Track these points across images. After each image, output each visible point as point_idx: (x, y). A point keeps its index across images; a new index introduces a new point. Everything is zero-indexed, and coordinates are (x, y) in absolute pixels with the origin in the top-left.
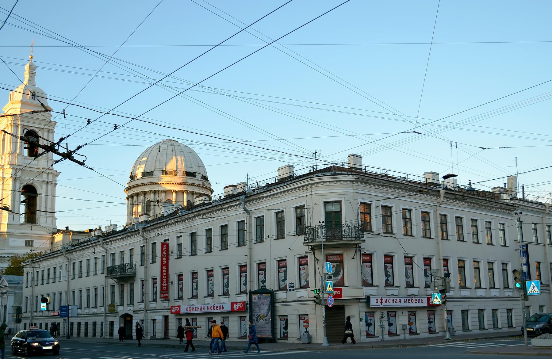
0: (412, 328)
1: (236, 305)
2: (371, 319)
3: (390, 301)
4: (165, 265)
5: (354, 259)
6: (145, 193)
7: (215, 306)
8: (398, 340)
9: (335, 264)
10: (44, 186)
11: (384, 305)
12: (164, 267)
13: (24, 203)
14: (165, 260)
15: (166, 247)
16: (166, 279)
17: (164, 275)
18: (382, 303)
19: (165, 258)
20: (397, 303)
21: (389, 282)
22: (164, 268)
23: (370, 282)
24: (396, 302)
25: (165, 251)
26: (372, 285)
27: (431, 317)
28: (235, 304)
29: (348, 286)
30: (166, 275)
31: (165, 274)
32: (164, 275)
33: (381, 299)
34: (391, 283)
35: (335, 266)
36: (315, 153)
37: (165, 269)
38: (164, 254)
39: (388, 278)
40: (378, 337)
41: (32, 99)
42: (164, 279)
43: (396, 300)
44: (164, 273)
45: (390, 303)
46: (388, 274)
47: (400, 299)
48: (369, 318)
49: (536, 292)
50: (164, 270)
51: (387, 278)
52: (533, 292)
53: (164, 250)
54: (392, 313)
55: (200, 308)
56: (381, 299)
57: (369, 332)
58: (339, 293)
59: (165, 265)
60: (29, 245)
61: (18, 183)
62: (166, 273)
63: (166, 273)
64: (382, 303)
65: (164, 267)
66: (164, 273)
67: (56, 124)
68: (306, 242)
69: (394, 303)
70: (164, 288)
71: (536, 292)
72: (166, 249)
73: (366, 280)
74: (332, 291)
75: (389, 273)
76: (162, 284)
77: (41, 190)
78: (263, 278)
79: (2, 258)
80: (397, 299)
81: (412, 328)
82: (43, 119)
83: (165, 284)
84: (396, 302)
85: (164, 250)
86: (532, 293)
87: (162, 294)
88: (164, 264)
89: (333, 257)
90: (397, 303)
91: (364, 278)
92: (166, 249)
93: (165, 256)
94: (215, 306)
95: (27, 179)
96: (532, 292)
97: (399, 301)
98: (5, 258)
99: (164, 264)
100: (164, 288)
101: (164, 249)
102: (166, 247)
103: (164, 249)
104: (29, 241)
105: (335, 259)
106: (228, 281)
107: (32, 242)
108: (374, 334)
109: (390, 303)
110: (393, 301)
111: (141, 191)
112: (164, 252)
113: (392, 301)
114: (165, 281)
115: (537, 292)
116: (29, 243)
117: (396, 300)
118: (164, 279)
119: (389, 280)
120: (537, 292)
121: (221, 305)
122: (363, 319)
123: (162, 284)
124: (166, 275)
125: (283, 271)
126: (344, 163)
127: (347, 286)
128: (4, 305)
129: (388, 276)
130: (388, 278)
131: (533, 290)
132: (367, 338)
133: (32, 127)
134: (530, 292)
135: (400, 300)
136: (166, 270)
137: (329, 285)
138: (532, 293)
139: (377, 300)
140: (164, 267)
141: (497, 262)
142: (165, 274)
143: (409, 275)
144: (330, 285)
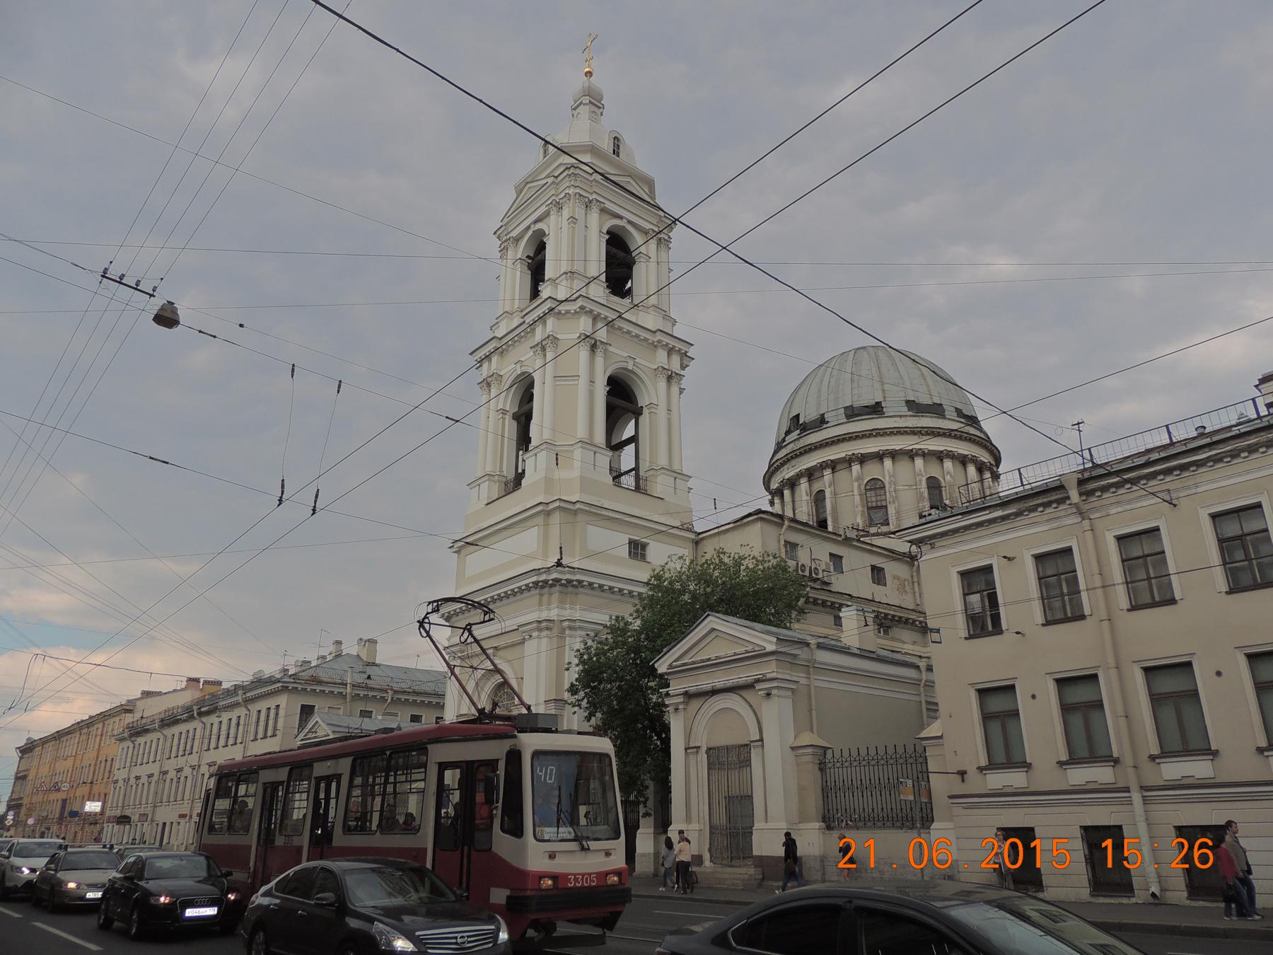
6: (863, 459)
10: (662, 384)
41: (614, 153)
61: (599, 360)
77: (650, 393)
79: (570, 589)
95: (622, 355)
98: (581, 590)
107: (644, 546)
111: (853, 454)
116: (637, 550)
128: (704, 749)
133: (621, 217)
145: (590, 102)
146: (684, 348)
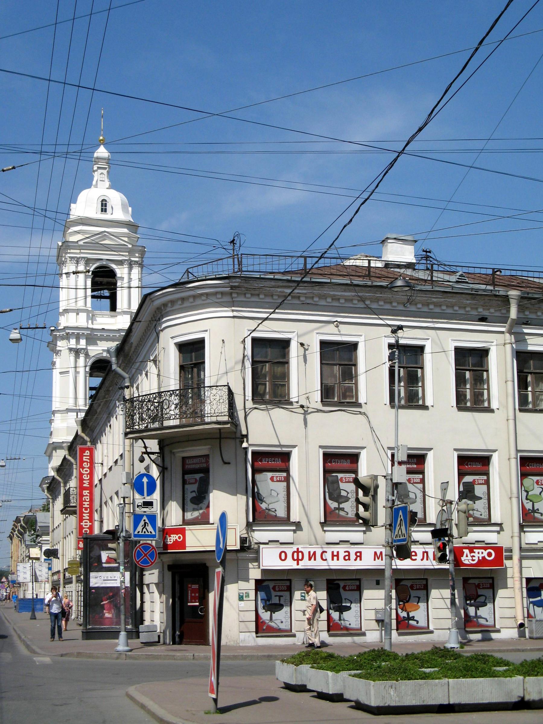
0: (413, 617)
2: (280, 597)
3: (328, 556)
5: (229, 463)
8: (233, 647)
9: (198, 476)
11: (306, 564)
12: (86, 492)
14: (86, 478)
15: (88, 454)
16: (88, 515)
17: (84, 506)
18: (298, 560)
19: (87, 474)
20: (349, 559)
21: (342, 513)
22: (85, 494)
23: (281, 513)
24: (347, 558)
26: (286, 521)
27: (479, 593)
29: (213, 524)
30: (88, 506)
31: (87, 505)
32: (84, 506)
33: (298, 551)
34: (350, 515)
35: (198, 480)
36: (233, 242)
37: (87, 496)
38: (86, 466)
39: (339, 503)
40: (294, 636)
41: (102, 211)
42: (84, 515)
43: (347, 554)
44: (84, 503)
45: (326, 560)
46: (339, 496)
47: (360, 553)
48: (273, 593)
49: (148, 532)
50: (84, 497)
51: (337, 504)
52: (145, 532)
53: (84, 460)
54: (484, 581)
56: (298, 551)
57: (272, 624)
58: (179, 538)
59: (86, 489)
62: (88, 503)
63: (88, 503)
64: (298, 560)
66: (84, 503)
69: (338, 559)
71: (148, 532)
72: (88, 457)
73: (269, 510)
74: (153, 533)
75: (343, 493)
76: (81, 524)
80: (349, 552)
81: (413, 617)
82: (117, 243)
83: (87, 522)
84: (347, 558)
85: (84, 460)
86: (143, 533)
88: (84, 485)
89: (195, 461)
90: (349, 559)
91: (264, 506)
92: (88, 457)
93: (86, 471)
96: (143, 532)
97: (357, 556)
99: (84, 485)
101: (84, 457)
102: (88, 454)
103: (84, 457)
105: (197, 466)
108: (288, 627)
109: (326, 560)
110: (338, 556)
112: (86, 463)
113: (333, 556)
114: (88, 518)
115: (150, 533)
117: (347, 554)
118: (84, 515)
119: (344, 508)
120: (150, 533)
122: (248, 595)
123: (91, 524)
124: (88, 506)
126: (242, 254)
127: (212, 523)
129: (340, 501)
130: (339, 503)
131: (145, 529)
132: (257, 637)
134: (139, 532)
135: (358, 554)
136: (88, 497)
137: (142, 523)
138: (143, 533)
139: (425, 554)
140: (86, 492)
141: (499, 456)
142: (87, 505)
143: (412, 496)
144: (147, 521)
145: (98, 167)
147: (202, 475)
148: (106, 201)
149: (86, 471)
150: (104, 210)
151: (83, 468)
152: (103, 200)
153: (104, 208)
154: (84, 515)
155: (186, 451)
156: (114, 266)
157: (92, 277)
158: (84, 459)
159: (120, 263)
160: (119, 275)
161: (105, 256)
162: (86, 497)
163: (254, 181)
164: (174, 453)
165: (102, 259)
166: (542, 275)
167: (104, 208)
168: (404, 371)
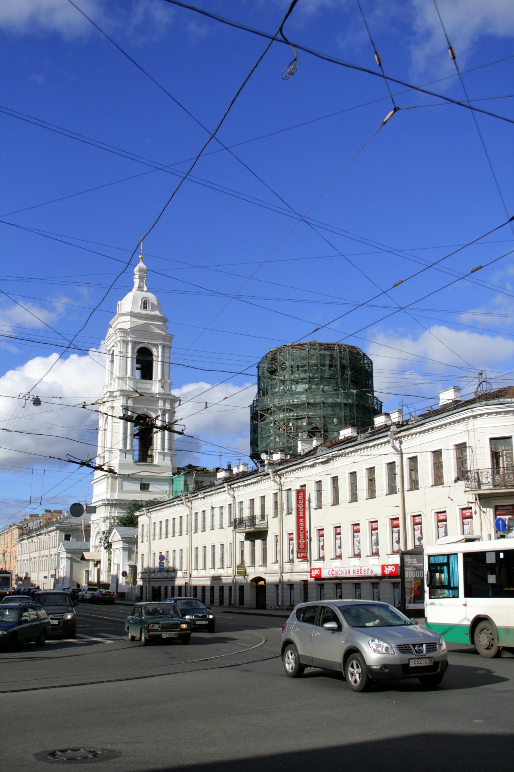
1: (314, 571)
4: (301, 518)
7: (363, 569)
13: (138, 437)
14: (301, 511)
25: (301, 500)
28: (386, 567)
36: (481, 374)
37: (302, 522)
38: (301, 503)
41: (144, 308)
53: (300, 498)
55: (344, 571)
59: (301, 518)
60: (144, 489)
65: (300, 520)
67: (172, 338)
68: (467, 489)
70: (302, 546)
78: (420, 535)
87: (299, 554)
88: (300, 515)
93: (301, 506)
94: (363, 569)
100: (302, 546)
101: (300, 497)
102: (302, 495)
104: (145, 484)
106: (377, 538)
112: (300, 501)
114: (303, 537)
121: (370, 568)
125: (443, 526)
146: (170, 398)
147: (510, 516)
148: (146, 301)
149: (301, 506)
150: (145, 308)
151: (299, 504)
152: (145, 301)
153: (145, 306)
154: (301, 535)
155: (309, 499)
156: (150, 347)
157: (137, 354)
158: (300, 498)
159: (156, 346)
160: (155, 353)
161: (146, 342)
162: (301, 524)
163: (510, 316)
164: (491, 503)
165: (144, 343)
166: (511, 377)
167: (145, 306)
168: (131, 425)
